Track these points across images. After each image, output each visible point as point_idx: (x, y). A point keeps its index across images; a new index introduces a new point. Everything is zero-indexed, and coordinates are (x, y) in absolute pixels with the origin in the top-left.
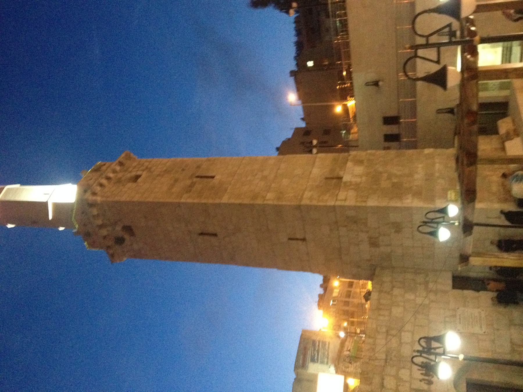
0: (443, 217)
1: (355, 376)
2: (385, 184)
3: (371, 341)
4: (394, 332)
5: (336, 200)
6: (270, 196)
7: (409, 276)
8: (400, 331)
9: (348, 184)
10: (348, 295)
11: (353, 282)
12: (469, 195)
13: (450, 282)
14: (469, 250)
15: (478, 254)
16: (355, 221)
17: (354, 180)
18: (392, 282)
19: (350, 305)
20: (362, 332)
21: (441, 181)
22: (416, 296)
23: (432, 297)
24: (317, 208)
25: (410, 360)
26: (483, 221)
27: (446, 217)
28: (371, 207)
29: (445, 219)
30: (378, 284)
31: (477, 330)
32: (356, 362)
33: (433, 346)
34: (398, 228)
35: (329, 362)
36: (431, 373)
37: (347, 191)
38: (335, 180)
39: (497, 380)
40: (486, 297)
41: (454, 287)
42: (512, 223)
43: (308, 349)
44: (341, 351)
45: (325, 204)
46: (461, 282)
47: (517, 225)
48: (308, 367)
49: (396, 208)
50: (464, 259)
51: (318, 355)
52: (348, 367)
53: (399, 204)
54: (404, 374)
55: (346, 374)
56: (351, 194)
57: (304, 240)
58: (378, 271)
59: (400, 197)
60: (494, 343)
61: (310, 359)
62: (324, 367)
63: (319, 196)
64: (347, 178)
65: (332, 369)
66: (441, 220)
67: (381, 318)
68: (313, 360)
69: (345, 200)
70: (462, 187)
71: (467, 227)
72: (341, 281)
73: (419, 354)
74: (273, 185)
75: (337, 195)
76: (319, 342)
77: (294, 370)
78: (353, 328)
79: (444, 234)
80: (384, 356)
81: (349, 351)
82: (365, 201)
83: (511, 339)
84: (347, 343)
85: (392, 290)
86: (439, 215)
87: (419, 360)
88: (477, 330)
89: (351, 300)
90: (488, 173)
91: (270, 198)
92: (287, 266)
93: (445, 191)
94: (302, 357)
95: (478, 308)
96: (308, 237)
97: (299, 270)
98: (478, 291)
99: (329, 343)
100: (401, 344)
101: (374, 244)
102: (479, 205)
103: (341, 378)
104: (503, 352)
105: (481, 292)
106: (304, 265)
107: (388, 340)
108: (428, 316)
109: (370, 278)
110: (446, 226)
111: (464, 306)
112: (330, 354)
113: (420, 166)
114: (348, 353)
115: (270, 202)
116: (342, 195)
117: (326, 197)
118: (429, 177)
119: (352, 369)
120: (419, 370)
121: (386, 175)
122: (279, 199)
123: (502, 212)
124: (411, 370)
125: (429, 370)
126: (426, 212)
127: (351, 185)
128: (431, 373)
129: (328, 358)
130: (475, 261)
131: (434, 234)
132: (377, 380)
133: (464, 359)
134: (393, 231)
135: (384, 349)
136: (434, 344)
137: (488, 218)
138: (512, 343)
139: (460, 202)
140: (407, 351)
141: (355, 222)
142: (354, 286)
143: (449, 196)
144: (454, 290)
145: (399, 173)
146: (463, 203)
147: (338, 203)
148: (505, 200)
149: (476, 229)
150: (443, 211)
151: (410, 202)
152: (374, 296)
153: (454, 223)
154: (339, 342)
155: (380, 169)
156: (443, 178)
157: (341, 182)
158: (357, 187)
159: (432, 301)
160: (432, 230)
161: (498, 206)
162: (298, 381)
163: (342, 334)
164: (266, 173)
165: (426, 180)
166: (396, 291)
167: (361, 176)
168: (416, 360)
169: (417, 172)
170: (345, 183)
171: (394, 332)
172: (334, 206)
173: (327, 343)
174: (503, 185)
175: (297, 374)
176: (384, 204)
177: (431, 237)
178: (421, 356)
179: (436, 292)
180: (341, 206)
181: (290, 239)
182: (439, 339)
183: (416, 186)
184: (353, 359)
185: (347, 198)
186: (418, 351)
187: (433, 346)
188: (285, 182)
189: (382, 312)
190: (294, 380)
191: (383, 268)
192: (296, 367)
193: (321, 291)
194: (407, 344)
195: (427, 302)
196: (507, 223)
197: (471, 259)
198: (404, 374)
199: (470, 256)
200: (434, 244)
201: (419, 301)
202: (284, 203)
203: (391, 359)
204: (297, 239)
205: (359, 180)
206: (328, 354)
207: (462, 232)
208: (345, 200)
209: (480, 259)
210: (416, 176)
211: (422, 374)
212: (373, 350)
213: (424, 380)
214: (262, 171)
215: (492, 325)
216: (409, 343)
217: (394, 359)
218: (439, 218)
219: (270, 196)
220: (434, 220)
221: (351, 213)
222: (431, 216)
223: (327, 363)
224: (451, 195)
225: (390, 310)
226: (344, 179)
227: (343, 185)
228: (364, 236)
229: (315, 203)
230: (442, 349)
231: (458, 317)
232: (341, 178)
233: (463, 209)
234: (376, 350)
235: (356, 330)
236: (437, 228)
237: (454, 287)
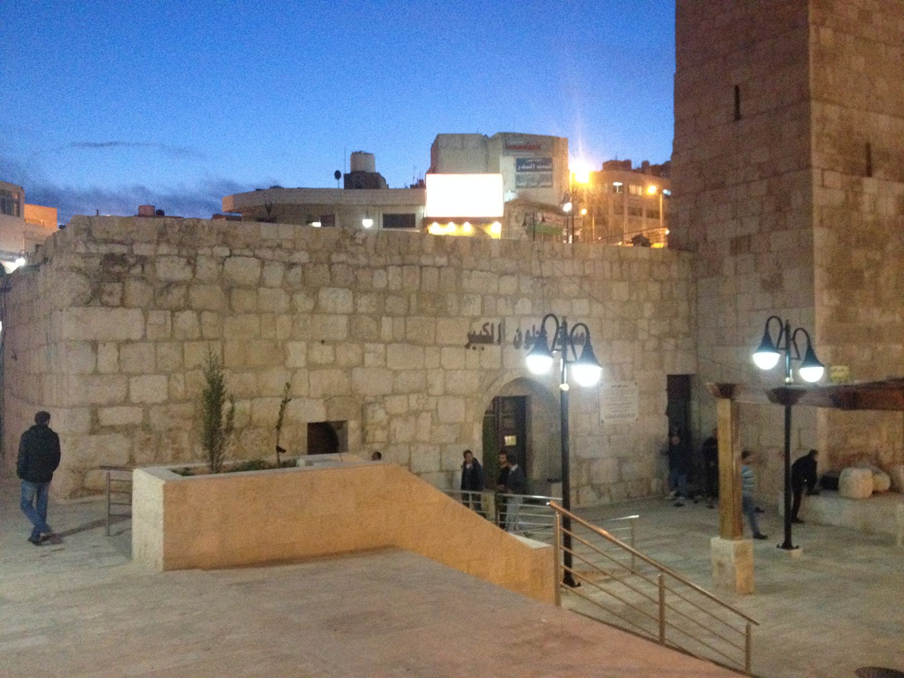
0: (799, 358)
1: (506, 230)
2: (859, 257)
3: (568, 252)
4: (587, 288)
5: (823, 170)
6: (827, 34)
7: (683, 307)
8: (591, 297)
9: (857, 189)
10: (635, 212)
11: (658, 218)
12: (845, 398)
13: (679, 371)
14: (742, 398)
15: (736, 412)
16: (782, 206)
17: (866, 199)
18: (670, 279)
19: (616, 216)
20: (575, 239)
21: (866, 355)
22: (650, 319)
23: (651, 344)
24: (804, 132)
25: (547, 312)
26: (795, 423)
27: (801, 362)
28: (812, 235)
29: (793, 361)
30: (656, 260)
31: (605, 411)
32: (527, 232)
33: (576, 347)
34: (773, 285)
35: (521, 190)
36: (532, 346)
37: (842, 189)
38: (864, 161)
39: (534, 439)
40: (658, 426)
41: (670, 377)
42: (793, 466)
43: (535, 154)
44: (545, 208)
45: (813, 147)
46: (680, 389)
47: (791, 473)
48: (508, 155)
49: (811, 280)
50: (726, 391)
51: (528, 170)
52: (517, 221)
53: (818, 283)
54: (525, 306)
55: (505, 221)
56: (838, 197)
57: (738, 117)
58: (686, 255)
59: (833, 285)
60: (588, 435)
61: (521, 157)
62: (512, 183)
63: (829, 135)
64: (870, 185)
65: (511, 196)
66: (794, 355)
67: (607, 266)
68: (519, 163)
69: (823, 186)
70: (857, 387)
71: (787, 395)
72: (657, 198)
73: (560, 325)
74: (850, 38)
75: (832, 170)
76: (551, 170)
77: (500, 133)
78: (581, 224)
79: (766, 361)
80: (547, 272)
81: (543, 220)
82: (821, 221)
83: (597, 459)
84: (554, 216)
85: (656, 281)
86: (803, 350)
87: (551, 328)
88: (605, 411)
89: (626, 216)
90: (884, 433)
91: (823, 36)
92: (683, 94)
93: (848, 361)
94: (521, 143)
95: (640, 414)
96: (741, 123)
97: (676, 116)
98: (668, 413)
99: (551, 186)
100: (568, 298)
101: (738, 245)
102: (822, 414)
103: (499, 212)
104: (580, 447)
105: (667, 418)
106: (684, 126)
107: (573, 279)
108: (619, 338)
109: (672, 242)
110: (782, 360)
111: (641, 393)
112: (534, 190)
113: (898, 318)
114: (540, 219)
115: (813, 38)
116: (834, 179)
117: (828, 149)
118: (873, 335)
119: (516, 228)
120: (534, 328)
121: (878, 257)
122: (821, 54)
123: (813, 453)
124: (533, 315)
125: (539, 342)
126: (807, 329)
127: (855, 194)
128: (532, 346)
129: (527, 187)
130: (724, 408)
131: (767, 344)
132: (510, 265)
133: (562, 392)
134: (765, 276)
135: (559, 274)
136: (579, 349)
137: (800, 431)
138: (592, 460)
139: (829, 384)
140: (560, 308)
141: (778, 209)
142: (651, 220)
143: (839, 368)
144: (666, 378)
145: (882, 280)
146: (829, 389)
147: (816, 174)
148: (832, 457)
149: (780, 409)
150: (811, 359)
151: (824, 303)
152: (643, 252)
153: (788, 375)
154: (557, 204)
155: (890, 247)
156: (873, 358)
157: (862, 175)
158: (851, 205)
159: (643, 347)
160: (774, 340)
161: (822, 446)
162: (485, 141)
163: (567, 207)
164: (877, 18)
165: (869, 330)
166: (654, 288)
167: (874, 211)
168: (550, 322)
169: (884, 311)
170: (859, 183)
171: (587, 288)
172: (809, 166)
173: (549, 184)
174: (861, 455)
175: (494, 139)
176: (818, 257)
177: (759, 339)
178: (558, 328)
179: (658, 349)
180: (810, 176)
181: (737, 89)
182: (589, 355)
183: (857, 313)
184: (531, 227)
185: (827, 188)
186: (565, 324)
187: (576, 347)
188: (859, 63)
189: (616, 267)
190: (483, 134)
191: (693, 263)
192: (505, 135)
193: (636, 164)
194: (571, 308)
195: (642, 336)
196: (793, 461)
197: (727, 402)
198: (525, 306)
199: (732, 400)
200: (743, 344)
201: (643, 324)
202: (812, 66)
203: (543, 285)
204: (737, 102)
205: (866, 207)
206: (533, 187)
207: (776, 386)
208: (823, 186)
209: (729, 415)
210: (876, 312)
211: (528, 332)
212: (554, 256)
213: (520, 335)
214: (882, 10)
215: (616, 433)
216: (578, 310)
217: (546, 289)
218: (797, 351)
219: (827, 34)
220: (792, 343)
221: (797, 201)
222: (801, 339)
223: (518, 187)
224: (841, 372)
225: (621, 279)
226: (867, 181)
227: (855, 178)
228: (752, 226)
229: (815, 128)
230: (573, 359)
231: (623, 383)
232: (869, 173)
233: (815, 389)
234: (555, 262)
235: (578, 229)
236: (776, 349)
237: (670, 377)
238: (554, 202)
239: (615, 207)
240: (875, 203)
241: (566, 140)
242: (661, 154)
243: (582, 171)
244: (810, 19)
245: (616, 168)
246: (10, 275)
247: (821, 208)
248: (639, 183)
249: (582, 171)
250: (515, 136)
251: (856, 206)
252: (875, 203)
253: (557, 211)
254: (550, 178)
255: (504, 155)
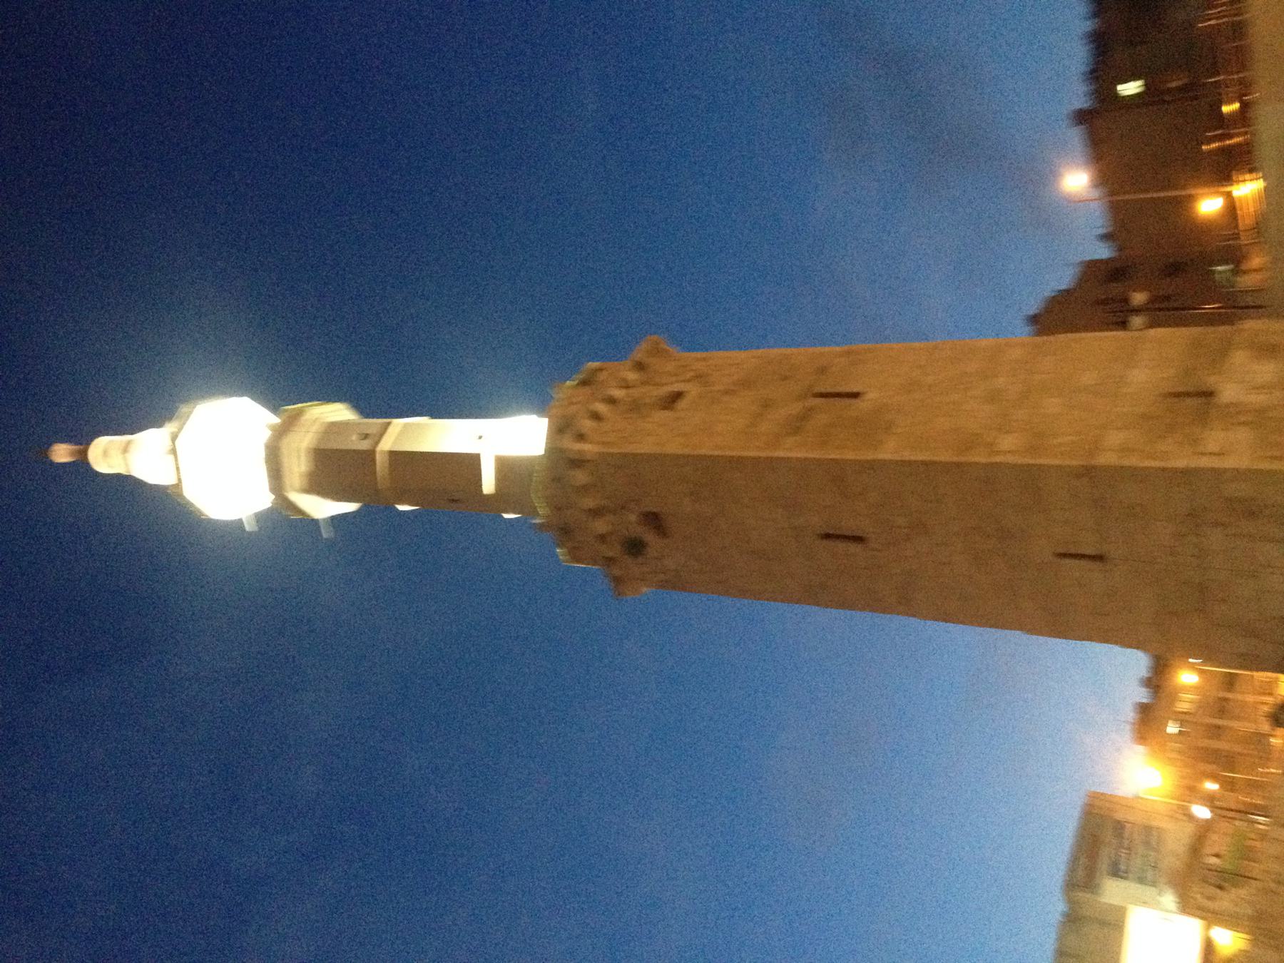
1: (1230, 921)
6: (1007, 442)
43: (1104, 842)
44: (1196, 848)
55: (1212, 916)
57: (1099, 558)
62: (1149, 892)
64: (1229, 392)
65: (1169, 899)
68: (1116, 873)
81: (1217, 856)
115: (1010, 459)
116: (1215, 438)
147: (1205, 462)
162: (1073, 920)
175: (1072, 903)
184: (1225, 879)
193: (1142, 695)
219: (1007, 442)
221: (1241, 489)
229: (1133, 461)
232: (1208, 394)
238: (1189, 829)
239: (1210, 738)
240: (1258, 388)
241: (1095, 796)
242: (1137, 662)
243: (1143, 777)
244: (983, 460)
245: (1147, 720)
246: (52, 463)
247: (1277, 679)
248: (1173, 696)
249: (1143, 777)
250: (1072, 870)
251: (1261, 412)
252: (1258, 388)
253: (1204, 829)
254: (1148, 829)
255: (1097, 894)
